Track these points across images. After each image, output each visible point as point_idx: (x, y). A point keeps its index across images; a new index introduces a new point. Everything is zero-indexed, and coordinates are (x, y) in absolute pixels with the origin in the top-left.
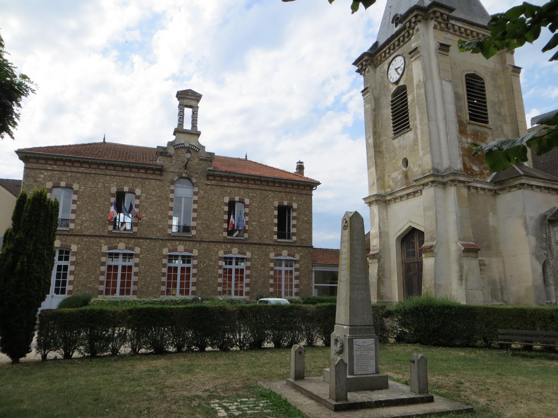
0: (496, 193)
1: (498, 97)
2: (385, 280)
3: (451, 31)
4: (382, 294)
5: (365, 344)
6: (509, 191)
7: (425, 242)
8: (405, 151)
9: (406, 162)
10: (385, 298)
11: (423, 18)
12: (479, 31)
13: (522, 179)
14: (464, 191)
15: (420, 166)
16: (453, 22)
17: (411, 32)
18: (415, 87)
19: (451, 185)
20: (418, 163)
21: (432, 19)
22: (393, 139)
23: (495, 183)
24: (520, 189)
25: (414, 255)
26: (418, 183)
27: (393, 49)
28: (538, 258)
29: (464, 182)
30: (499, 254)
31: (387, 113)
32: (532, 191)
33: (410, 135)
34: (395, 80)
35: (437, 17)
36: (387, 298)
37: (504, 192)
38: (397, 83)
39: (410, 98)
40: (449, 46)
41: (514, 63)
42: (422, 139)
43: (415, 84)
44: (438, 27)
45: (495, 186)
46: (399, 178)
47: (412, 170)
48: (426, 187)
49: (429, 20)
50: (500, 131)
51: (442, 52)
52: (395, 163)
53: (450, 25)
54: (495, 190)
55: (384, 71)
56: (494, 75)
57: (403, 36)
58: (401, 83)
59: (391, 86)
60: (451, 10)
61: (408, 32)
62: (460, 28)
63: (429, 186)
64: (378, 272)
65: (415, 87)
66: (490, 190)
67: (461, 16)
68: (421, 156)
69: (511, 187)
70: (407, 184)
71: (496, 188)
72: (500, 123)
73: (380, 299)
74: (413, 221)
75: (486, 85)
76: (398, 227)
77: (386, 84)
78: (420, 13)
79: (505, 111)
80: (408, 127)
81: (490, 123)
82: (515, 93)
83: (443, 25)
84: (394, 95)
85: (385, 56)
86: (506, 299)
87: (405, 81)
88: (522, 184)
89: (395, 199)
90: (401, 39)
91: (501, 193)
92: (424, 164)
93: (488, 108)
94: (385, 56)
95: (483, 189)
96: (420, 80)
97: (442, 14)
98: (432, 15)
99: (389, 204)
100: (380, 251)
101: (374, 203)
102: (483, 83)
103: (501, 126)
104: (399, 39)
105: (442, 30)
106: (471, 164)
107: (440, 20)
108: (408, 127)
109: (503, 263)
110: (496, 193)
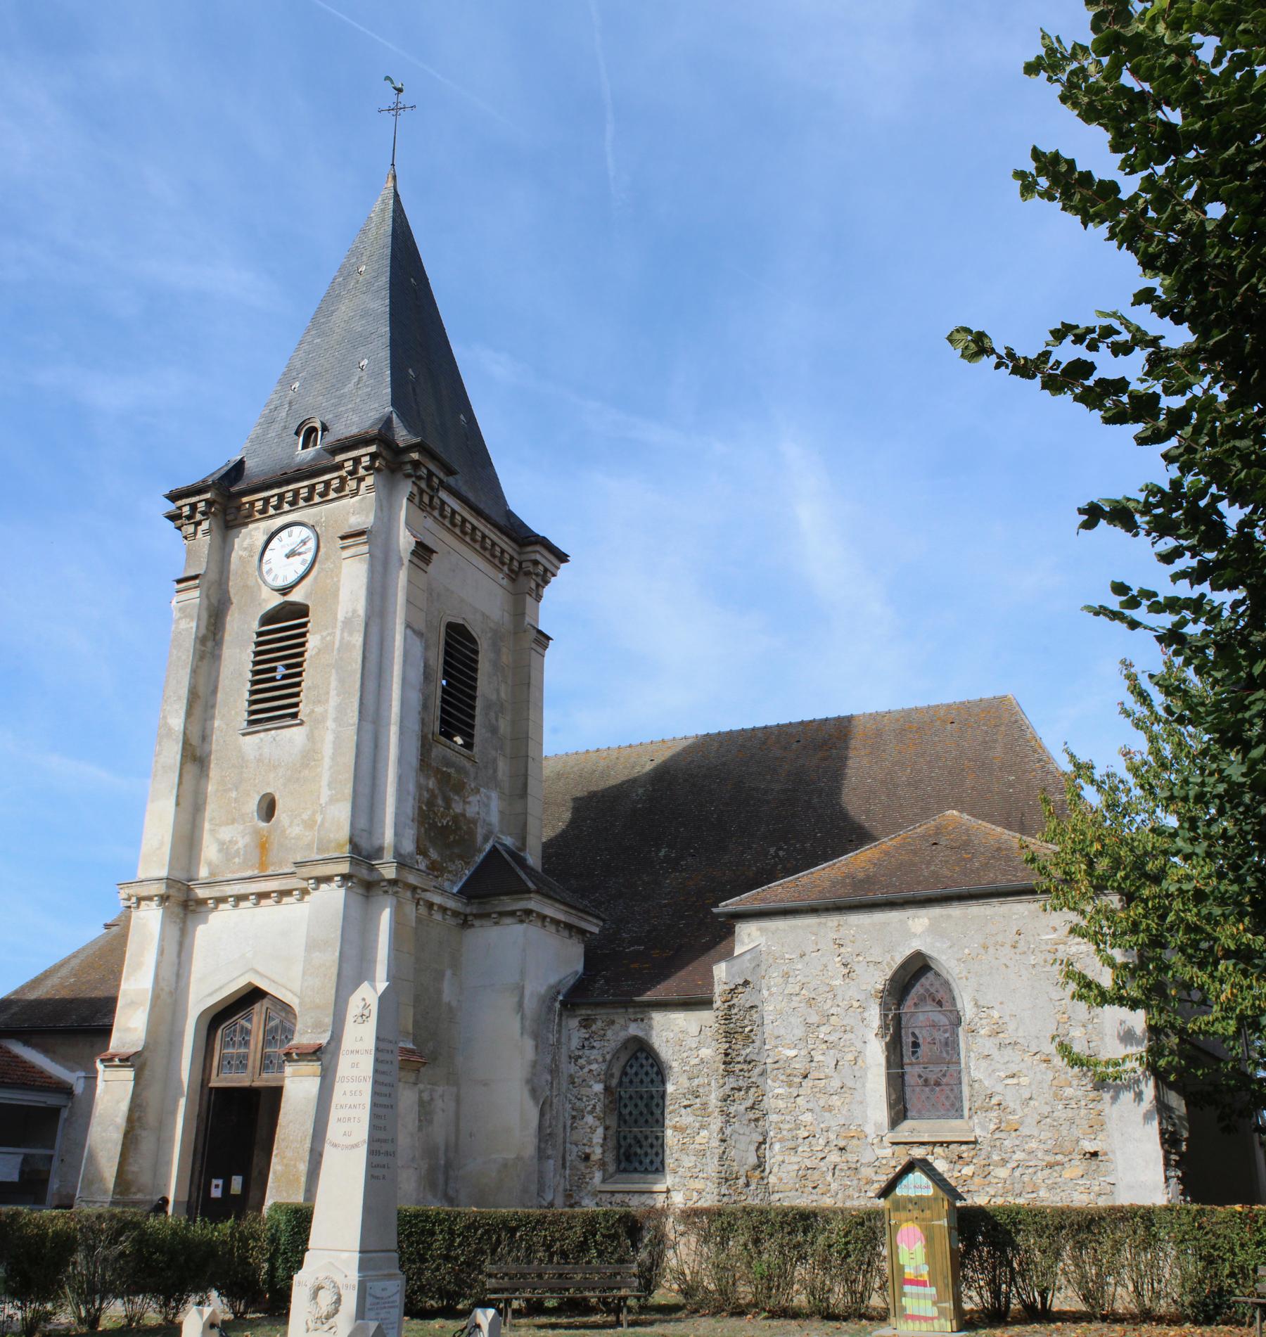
0: (465, 921)
1: (498, 691)
2: (144, 1134)
3: (436, 513)
4: (130, 1177)
5: (385, 1294)
6: (496, 923)
7: (296, 1035)
8: (272, 775)
9: (268, 808)
10: (133, 1190)
11: (387, 466)
12: (487, 532)
13: (530, 898)
14: (410, 909)
15: (309, 824)
16: (443, 495)
17: (352, 484)
18: (339, 624)
19: (386, 892)
20: (305, 817)
21: (408, 476)
22: (244, 735)
23: (470, 898)
24: (522, 921)
25: (245, 1066)
26: (305, 872)
27: (292, 504)
28: (534, 1092)
29: (414, 889)
30: (453, 1079)
31: (238, 659)
32: (542, 931)
33: (291, 738)
34: (280, 583)
35: (420, 478)
36: (139, 1191)
37: (484, 922)
38: (285, 591)
39: (313, 642)
40: (433, 552)
41: (537, 622)
42: (333, 758)
43: (340, 617)
44: (417, 500)
45: (467, 904)
46: (241, 844)
47: (283, 831)
48: (323, 886)
49: (400, 475)
50: (491, 771)
51: (415, 560)
52: (236, 800)
53: (436, 500)
54: (466, 916)
55: (251, 546)
56: (497, 637)
57: (327, 484)
58: (296, 596)
59: (265, 592)
60: (450, 472)
61: (343, 480)
62: (454, 512)
63: (334, 885)
64: (131, 1110)
65: (339, 624)
66: (456, 914)
67: (465, 490)
68: (323, 801)
69: (502, 914)
70: (263, 865)
71: (468, 910)
72: (493, 753)
73: (121, 1193)
74: (260, 969)
75: (480, 657)
76: (209, 986)
77: (251, 582)
78: (384, 453)
79: (504, 726)
80: (295, 715)
81: (475, 749)
82: (532, 689)
83: (426, 499)
84: (268, 619)
85: (263, 511)
86: (451, 1193)
87: (308, 596)
88: (528, 912)
89: (220, 900)
90: (320, 488)
91: (477, 923)
92: (327, 825)
93: (478, 711)
94: (263, 511)
95: (443, 909)
96: (354, 611)
97: (431, 474)
98: (409, 469)
99: (194, 912)
100: (145, 1047)
101: (154, 904)
102: (476, 652)
103: (495, 760)
104: (313, 486)
105: (421, 506)
106: (428, 844)
107: (423, 485)
108: (295, 715)
109: (458, 1101)
110: (465, 921)
